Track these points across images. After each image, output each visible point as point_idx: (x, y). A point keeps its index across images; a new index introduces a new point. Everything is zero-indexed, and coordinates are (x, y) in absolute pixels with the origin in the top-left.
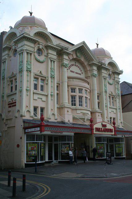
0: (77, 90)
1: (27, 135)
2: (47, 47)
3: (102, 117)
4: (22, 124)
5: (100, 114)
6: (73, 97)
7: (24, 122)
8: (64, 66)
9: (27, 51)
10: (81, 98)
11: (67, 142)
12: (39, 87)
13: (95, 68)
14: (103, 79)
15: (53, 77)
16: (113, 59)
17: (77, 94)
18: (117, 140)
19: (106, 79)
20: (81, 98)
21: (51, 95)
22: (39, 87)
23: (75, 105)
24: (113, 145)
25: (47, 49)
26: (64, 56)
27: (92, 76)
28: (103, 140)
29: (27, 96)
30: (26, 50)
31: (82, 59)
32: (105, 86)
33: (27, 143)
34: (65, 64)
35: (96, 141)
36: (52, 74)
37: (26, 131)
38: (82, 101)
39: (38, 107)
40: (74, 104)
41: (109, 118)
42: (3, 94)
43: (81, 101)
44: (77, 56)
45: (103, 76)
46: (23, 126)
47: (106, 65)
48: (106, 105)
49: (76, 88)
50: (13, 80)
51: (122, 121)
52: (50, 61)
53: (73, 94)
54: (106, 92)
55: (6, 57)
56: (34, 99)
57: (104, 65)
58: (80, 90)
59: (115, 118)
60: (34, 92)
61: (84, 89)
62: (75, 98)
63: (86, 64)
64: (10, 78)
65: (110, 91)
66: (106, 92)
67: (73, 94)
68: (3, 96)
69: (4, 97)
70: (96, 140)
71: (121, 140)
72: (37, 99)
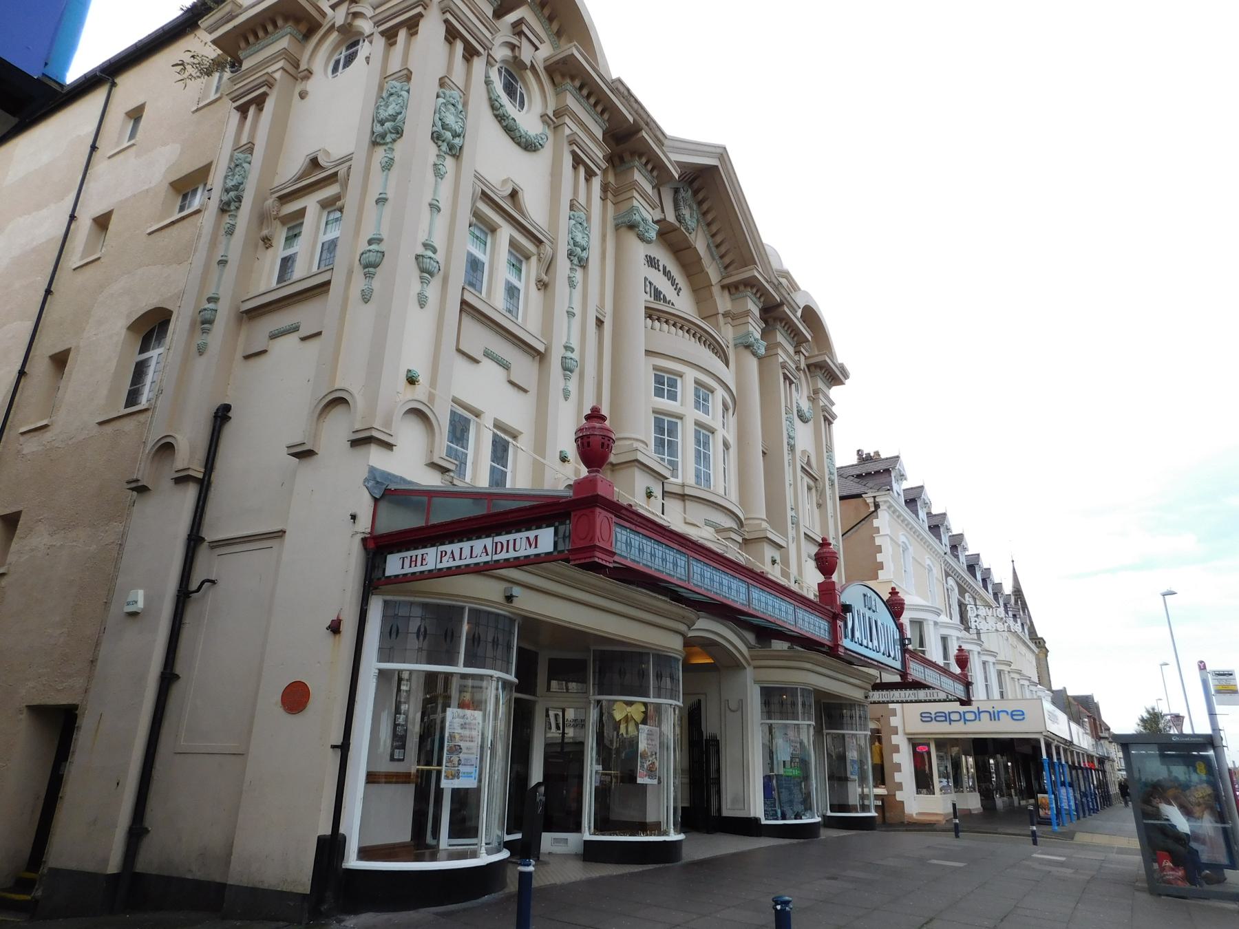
0: (686, 388)
1: (386, 603)
4: (364, 505)
7: (389, 494)
9: (448, 16)
10: (704, 432)
11: (460, 669)
15: (580, 260)
17: (684, 404)
20: (704, 432)
27: (741, 349)
28: (474, 640)
31: (700, 243)
33: (382, 674)
36: (579, 239)
37: (394, 565)
38: (707, 457)
42: (211, 306)
44: (679, 218)
46: (364, 525)
50: (301, 213)
52: (568, 161)
55: (276, 70)
56: (461, 347)
58: (702, 393)
61: (691, 375)
62: (672, 431)
63: (713, 273)
64: (284, 199)
66: (792, 448)
68: (208, 315)
69: (211, 322)
71: (659, 676)
72: (478, 355)
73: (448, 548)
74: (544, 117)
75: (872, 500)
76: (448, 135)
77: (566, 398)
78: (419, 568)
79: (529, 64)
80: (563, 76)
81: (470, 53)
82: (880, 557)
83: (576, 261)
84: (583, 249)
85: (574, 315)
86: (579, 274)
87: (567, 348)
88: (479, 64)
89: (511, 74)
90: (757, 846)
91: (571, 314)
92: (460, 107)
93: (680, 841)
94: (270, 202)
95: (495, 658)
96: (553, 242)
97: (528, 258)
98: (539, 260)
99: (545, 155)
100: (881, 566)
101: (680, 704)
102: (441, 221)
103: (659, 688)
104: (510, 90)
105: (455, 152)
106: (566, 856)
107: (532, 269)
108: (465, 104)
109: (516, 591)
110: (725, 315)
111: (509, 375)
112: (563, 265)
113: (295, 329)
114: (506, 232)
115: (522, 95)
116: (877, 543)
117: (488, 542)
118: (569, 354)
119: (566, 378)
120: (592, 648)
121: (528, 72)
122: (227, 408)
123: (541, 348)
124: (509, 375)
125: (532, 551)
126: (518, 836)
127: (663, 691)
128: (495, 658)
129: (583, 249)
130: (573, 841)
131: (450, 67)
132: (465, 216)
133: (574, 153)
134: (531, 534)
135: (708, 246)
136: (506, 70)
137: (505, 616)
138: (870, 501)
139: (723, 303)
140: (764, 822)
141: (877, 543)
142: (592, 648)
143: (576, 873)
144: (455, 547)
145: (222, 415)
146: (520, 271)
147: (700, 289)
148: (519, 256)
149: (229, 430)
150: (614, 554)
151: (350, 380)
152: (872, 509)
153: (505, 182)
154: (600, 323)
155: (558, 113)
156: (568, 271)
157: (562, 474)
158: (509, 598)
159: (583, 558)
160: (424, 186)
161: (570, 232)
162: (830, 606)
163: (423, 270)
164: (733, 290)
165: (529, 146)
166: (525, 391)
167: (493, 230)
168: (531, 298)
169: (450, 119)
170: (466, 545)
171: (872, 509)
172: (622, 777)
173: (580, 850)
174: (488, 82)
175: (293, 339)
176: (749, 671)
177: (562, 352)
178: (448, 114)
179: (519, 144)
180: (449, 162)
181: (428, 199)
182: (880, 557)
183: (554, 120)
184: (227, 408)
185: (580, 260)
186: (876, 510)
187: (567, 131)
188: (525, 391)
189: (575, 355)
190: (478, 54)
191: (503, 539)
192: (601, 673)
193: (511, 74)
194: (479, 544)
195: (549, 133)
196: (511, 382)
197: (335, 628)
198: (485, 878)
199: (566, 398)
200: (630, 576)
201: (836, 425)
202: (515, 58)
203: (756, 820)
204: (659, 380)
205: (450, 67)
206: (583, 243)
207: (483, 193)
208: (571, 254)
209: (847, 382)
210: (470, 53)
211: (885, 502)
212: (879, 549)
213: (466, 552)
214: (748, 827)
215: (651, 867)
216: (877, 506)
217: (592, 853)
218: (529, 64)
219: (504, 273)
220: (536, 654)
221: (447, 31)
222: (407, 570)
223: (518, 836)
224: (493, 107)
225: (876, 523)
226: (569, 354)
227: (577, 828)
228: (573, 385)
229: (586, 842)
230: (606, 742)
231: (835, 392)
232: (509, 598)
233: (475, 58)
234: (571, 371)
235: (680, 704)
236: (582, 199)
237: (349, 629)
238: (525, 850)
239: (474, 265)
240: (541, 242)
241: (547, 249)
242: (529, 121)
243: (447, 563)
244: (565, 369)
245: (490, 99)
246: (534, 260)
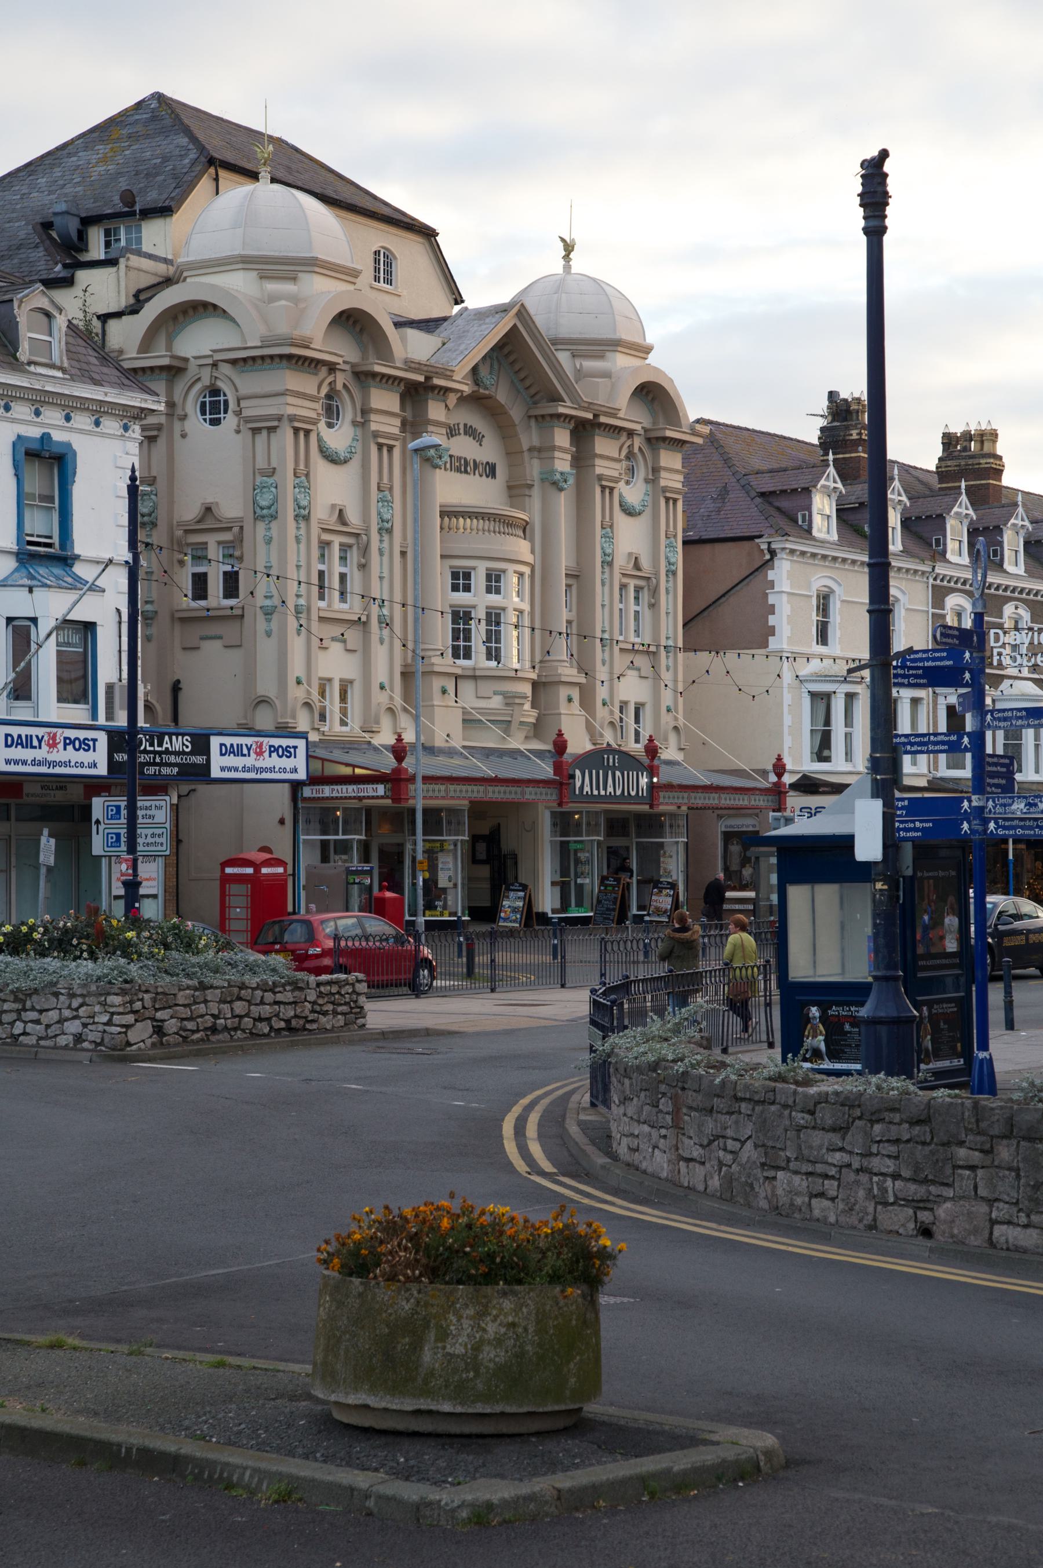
0: (479, 580)
2: (363, 377)
3: (582, 704)
5: (575, 694)
6: (461, 617)
8: (555, 483)
10: (494, 618)
11: (340, 837)
12: (216, 586)
13: (562, 437)
14: (598, 490)
16: (254, 274)
18: (650, 824)
19: (612, 489)
21: (298, 611)
22: (216, 586)
23: (468, 656)
24: (627, 849)
25: (655, 452)
26: (430, 401)
29: (269, 636)
30: (292, 418)
32: (609, 526)
34: (558, 476)
35: (554, 833)
39: (330, 680)
40: (462, 652)
41: (617, 705)
43: (493, 637)
45: (600, 478)
47: (457, 377)
48: (302, 601)
49: (474, 568)
51: (681, 721)
53: (461, 598)
54: (610, 564)
57: (607, 414)
59: (643, 705)
60: (321, 615)
61: (511, 568)
63: (516, 413)
65: (333, 506)
67: (461, 598)
70: (554, 825)
73: (335, 787)
77: (604, 665)
78: (321, 795)
82: (772, 620)
86: (386, 632)
94: (179, 533)
101: (466, 838)
110: (530, 450)
113: (220, 638)
116: (770, 602)
117: (355, 787)
122: (178, 681)
125: (375, 794)
134: (375, 786)
135: (512, 382)
138: (764, 547)
139: (529, 437)
140: (550, 915)
141: (770, 602)
144: (339, 787)
145: (176, 688)
147: (505, 430)
149: (182, 697)
151: (266, 687)
154: (403, 554)
156: (378, 543)
157: (387, 763)
164: (540, 419)
170: (344, 787)
171: (768, 557)
172: (710, 918)
175: (217, 644)
182: (772, 620)
184: (178, 681)
186: (772, 559)
191: (362, 786)
194: (350, 788)
196: (347, 650)
197: (282, 822)
199: (604, 665)
204: (455, 575)
212: (772, 609)
213: (344, 790)
216: (773, 553)
222: (314, 795)
225: (771, 575)
235: (466, 838)
237: (289, 822)
243: (335, 794)
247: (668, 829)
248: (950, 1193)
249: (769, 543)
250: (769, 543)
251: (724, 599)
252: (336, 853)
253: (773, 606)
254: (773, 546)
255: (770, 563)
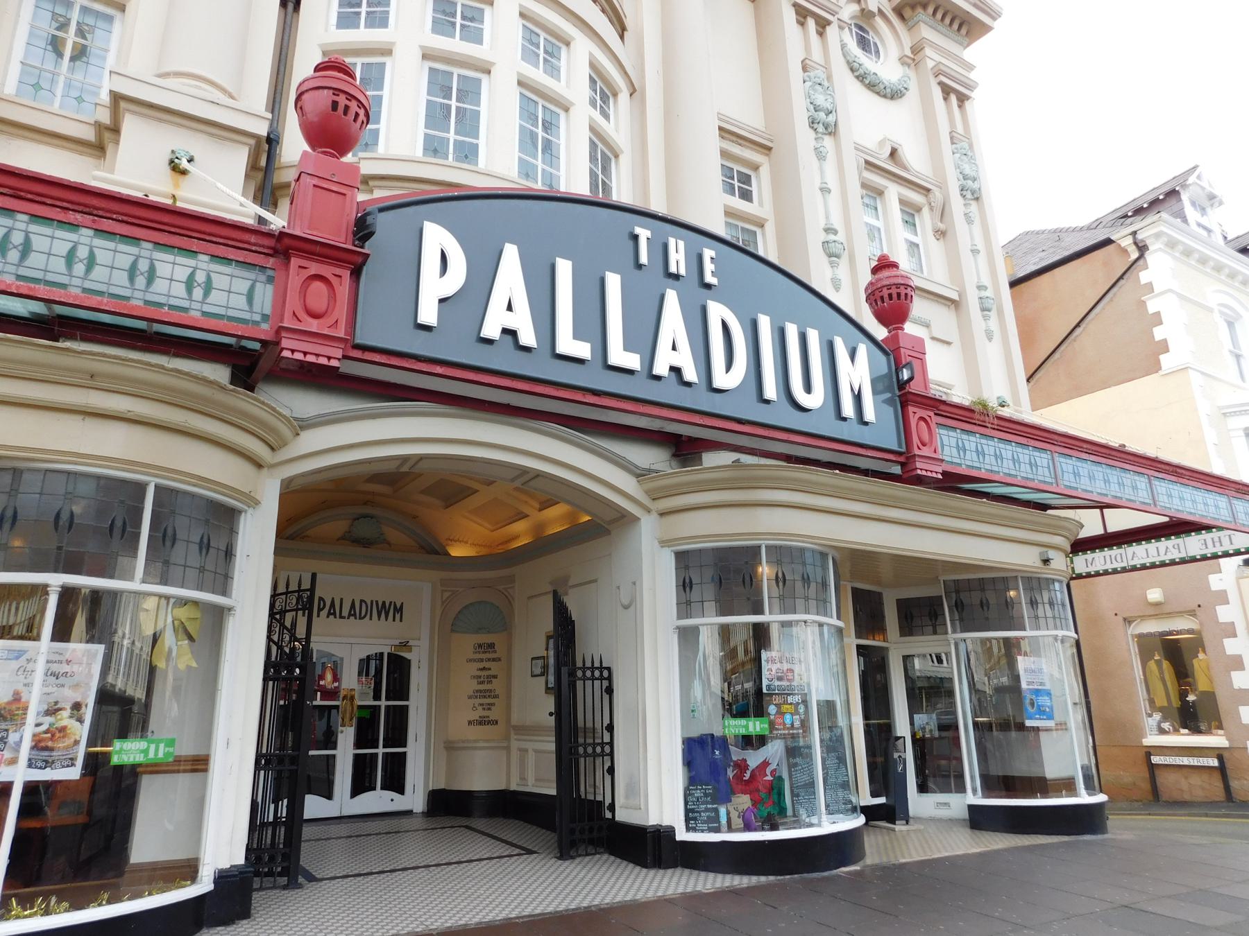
15: (973, 193)
36: (968, 171)
52: (937, 93)
71: (1033, 603)
74: (903, 61)
75: (1130, 240)
76: (822, 115)
77: (990, 339)
79: (876, 10)
80: (913, 7)
81: (823, 25)
82: (1159, 333)
83: (821, 129)
84: (974, 180)
85: (978, 252)
87: (980, 288)
88: (832, 31)
89: (861, 28)
90: (996, 847)
91: (975, 252)
92: (826, 84)
93: (1099, 806)
95: (807, 599)
96: (943, 186)
97: (919, 210)
98: (931, 209)
99: (912, 96)
100: (1164, 347)
102: (834, 199)
103: (1037, 617)
104: (863, 43)
105: (832, 130)
106: (952, 821)
107: (926, 220)
108: (829, 78)
109: (1052, 554)
111: (930, 332)
112: (957, 205)
114: (893, 192)
115: (875, 44)
118: (832, 237)
119: (986, 318)
120: (942, 579)
121: (878, 19)
123: (955, 296)
124: (930, 332)
126: (882, 800)
127: (1042, 621)
128: (807, 599)
129: (974, 180)
130: (957, 804)
131: (807, 48)
132: (855, 190)
133: (941, 84)
136: (856, 25)
137: (813, 551)
138: (1127, 242)
140: (682, 835)
142: (942, 579)
143: (967, 844)
146: (914, 225)
148: (910, 212)
150: (942, 461)
152: (1135, 255)
153: (881, 143)
155: (917, 49)
156: (963, 208)
158: (1046, 561)
159: (903, 470)
160: (810, 173)
161: (957, 167)
162: (904, 392)
163: (830, 255)
165: (894, 94)
166: (949, 343)
167: (880, 193)
168: (933, 250)
169: (820, 100)
171: (1135, 255)
173: (965, 814)
174: (843, 46)
176: (648, 530)
177: (823, 237)
178: (817, 96)
179: (885, 96)
180: (828, 142)
181: (818, 184)
182: (1159, 333)
183: (914, 57)
185: (973, 193)
186: (1141, 256)
187: (930, 64)
188: (949, 343)
189: (840, 237)
190: (829, 23)
192: (959, 606)
193: (861, 28)
195: (911, 73)
198: (838, 849)
199: (990, 339)
200: (953, 482)
201: (978, 104)
202: (863, 10)
203: (663, 835)
205: (807, 48)
206: (973, 174)
207: (867, 162)
208: (813, 122)
209: (996, 25)
210: (823, 25)
211: (1158, 236)
212: (1157, 319)
213: (1162, 551)
214: (648, 847)
215: (754, 880)
216: (1142, 249)
217: (979, 819)
218: (876, 10)
219: (902, 234)
220: (880, 594)
221: (797, 13)
223: (882, 800)
224: (852, 70)
225: (1144, 277)
226: (984, 294)
227: (961, 789)
228: (993, 324)
229: (972, 808)
230: (979, 686)
231: (976, 51)
232: (1046, 561)
233: (828, 29)
234: (989, 310)
236: (817, 55)
238: (888, 813)
239: (913, 246)
240: (928, 190)
241: (937, 194)
242: (888, 69)
244: (983, 310)
245: (848, 62)
246: (926, 210)
247: (1025, 610)
248: (1050, 724)
249: (1134, 233)
250: (1134, 233)
251: (1078, 331)
252: (923, 788)
253: (1158, 314)
254: (1140, 236)
255: (1141, 262)
